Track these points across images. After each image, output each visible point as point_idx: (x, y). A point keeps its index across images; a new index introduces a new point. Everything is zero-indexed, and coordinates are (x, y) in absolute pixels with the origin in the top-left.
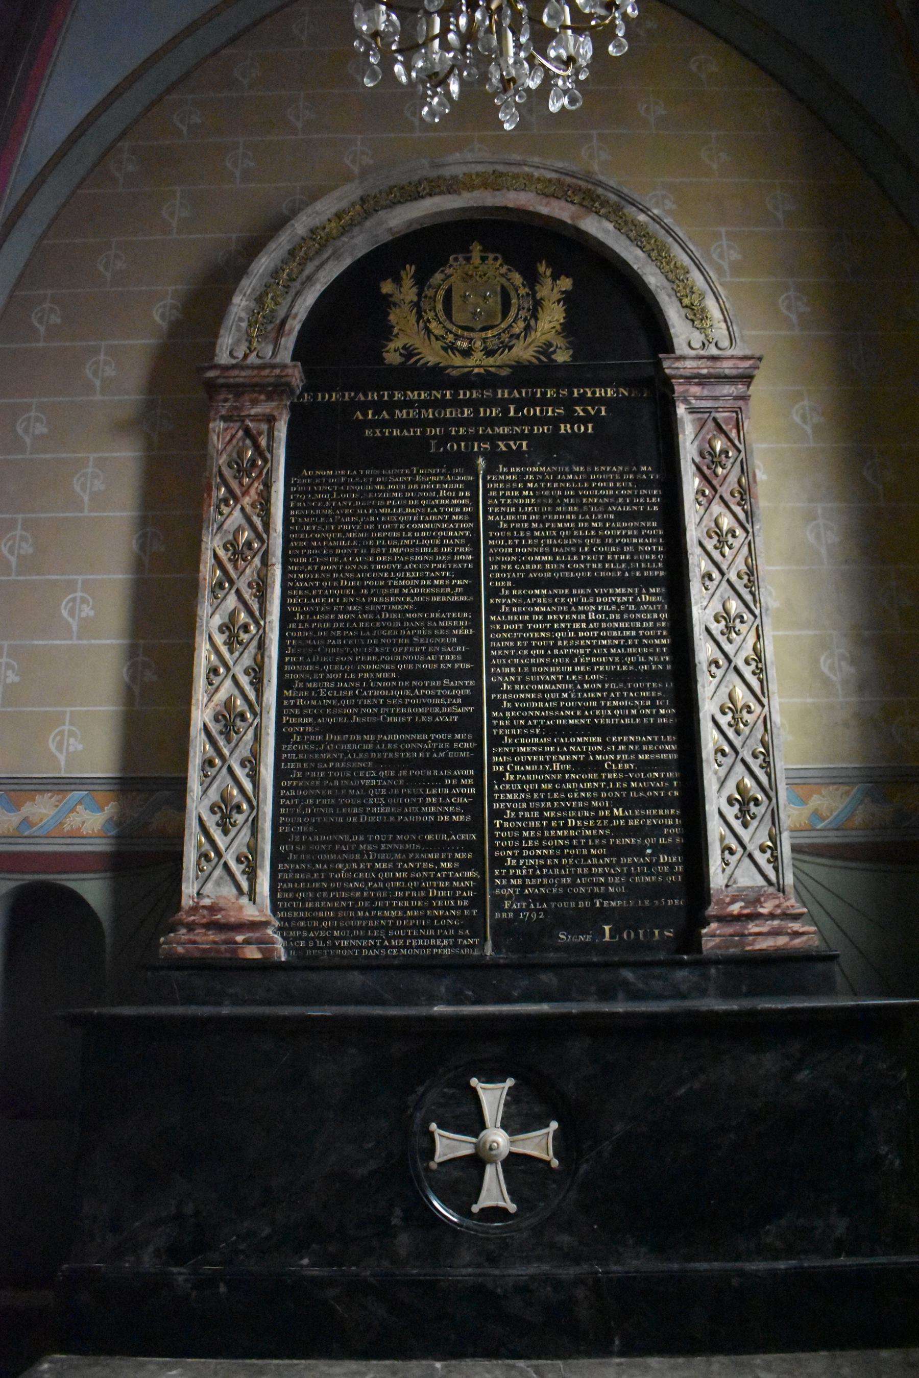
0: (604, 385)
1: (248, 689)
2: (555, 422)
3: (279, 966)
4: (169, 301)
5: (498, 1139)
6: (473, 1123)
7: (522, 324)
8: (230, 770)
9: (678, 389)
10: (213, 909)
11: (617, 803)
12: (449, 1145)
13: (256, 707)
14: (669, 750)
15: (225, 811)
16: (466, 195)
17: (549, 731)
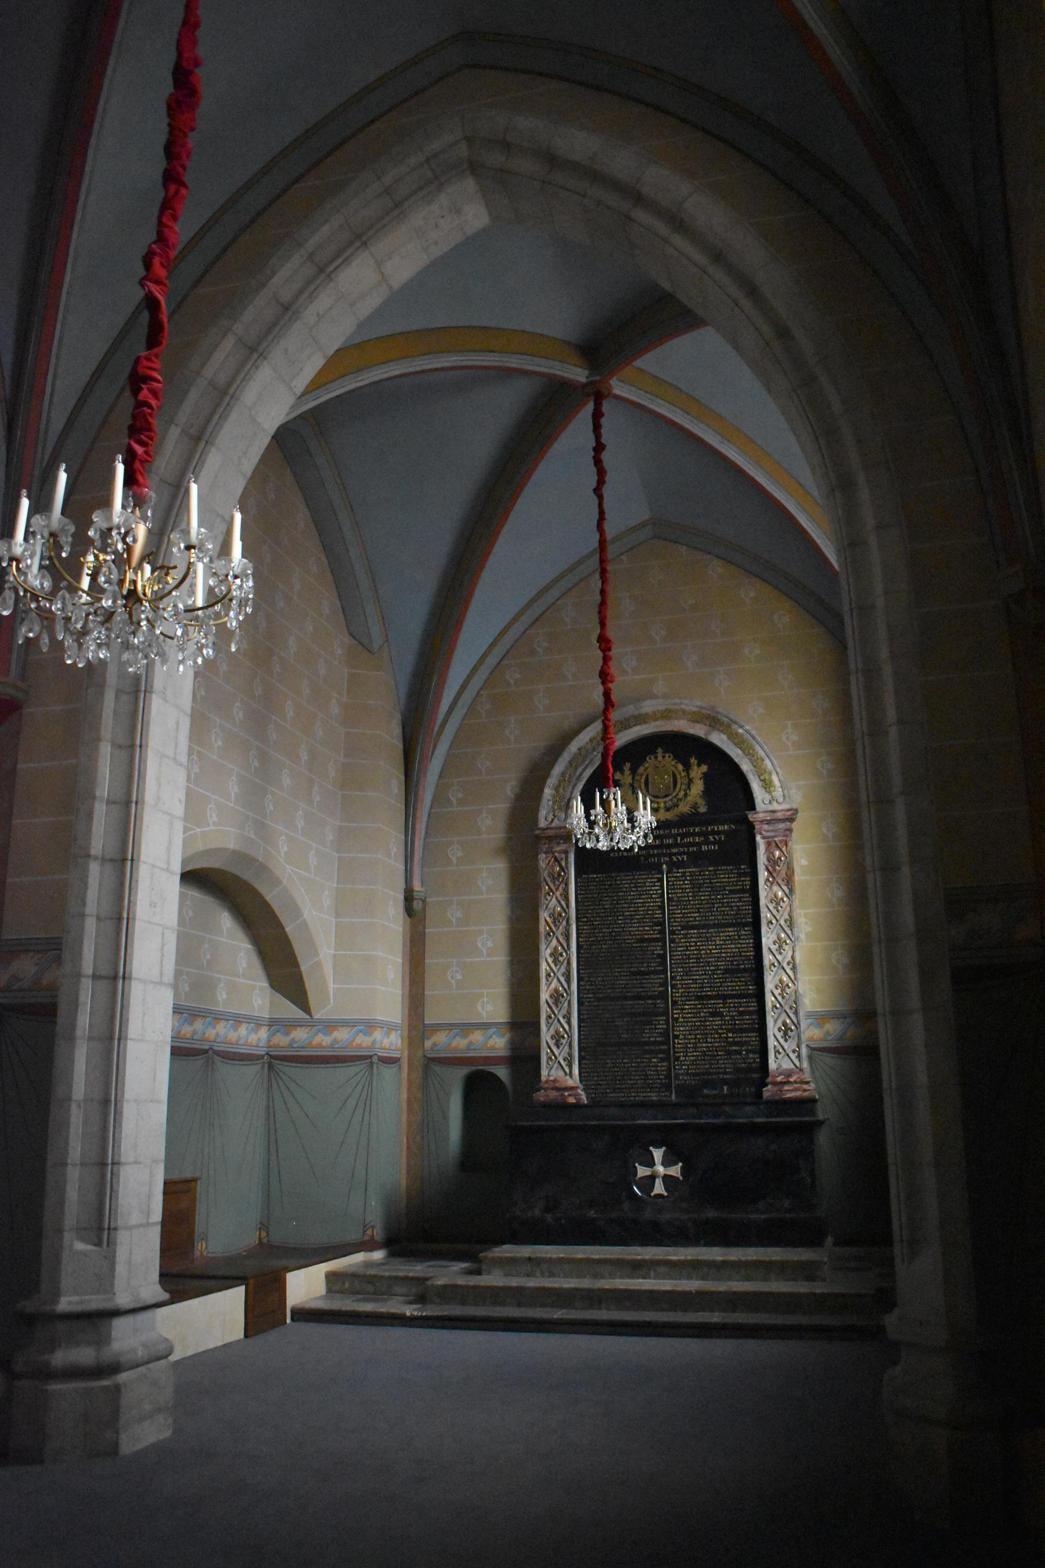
0: (723, 823)
1: (564, 983)
2: (699, 844)
3: (585, 1106)
4: (514, 783)
5: (660, 1169)
6: (651, 1164)
7: (682, 793)
8: (559, 1020)
9: (757, 827)
10: (555, 1081)
11: (729, 1031)
12: (642, 1171)
13: (568, 991)
14: (753, 1006)
15: (557, 1038)
16: (653, 724)
17: (700, 998)
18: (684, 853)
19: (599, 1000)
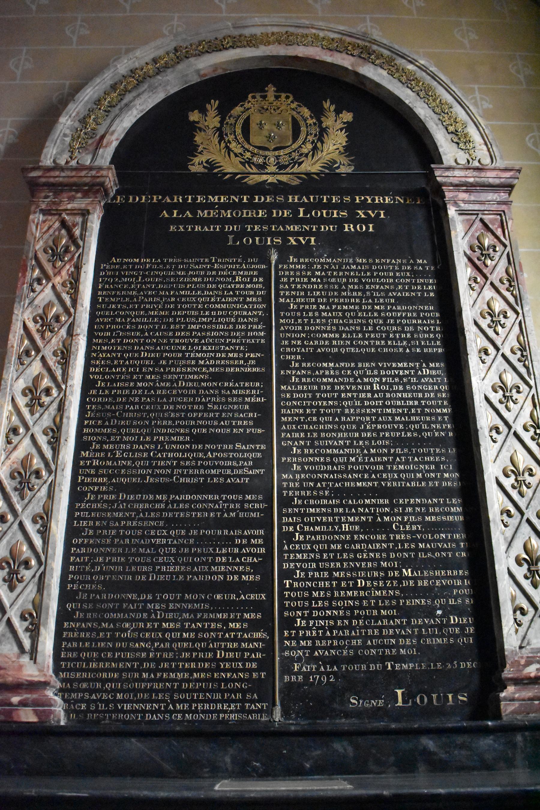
0: (383, 193)
2: (340, 222)
3: (58, 732)
7: (310, 146)
8: (21, 526)
11: (405, 563)
18: (310, 233)
19: (119, 488)
